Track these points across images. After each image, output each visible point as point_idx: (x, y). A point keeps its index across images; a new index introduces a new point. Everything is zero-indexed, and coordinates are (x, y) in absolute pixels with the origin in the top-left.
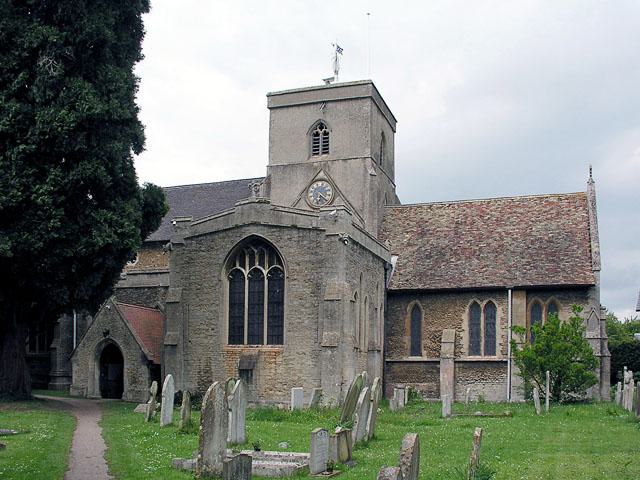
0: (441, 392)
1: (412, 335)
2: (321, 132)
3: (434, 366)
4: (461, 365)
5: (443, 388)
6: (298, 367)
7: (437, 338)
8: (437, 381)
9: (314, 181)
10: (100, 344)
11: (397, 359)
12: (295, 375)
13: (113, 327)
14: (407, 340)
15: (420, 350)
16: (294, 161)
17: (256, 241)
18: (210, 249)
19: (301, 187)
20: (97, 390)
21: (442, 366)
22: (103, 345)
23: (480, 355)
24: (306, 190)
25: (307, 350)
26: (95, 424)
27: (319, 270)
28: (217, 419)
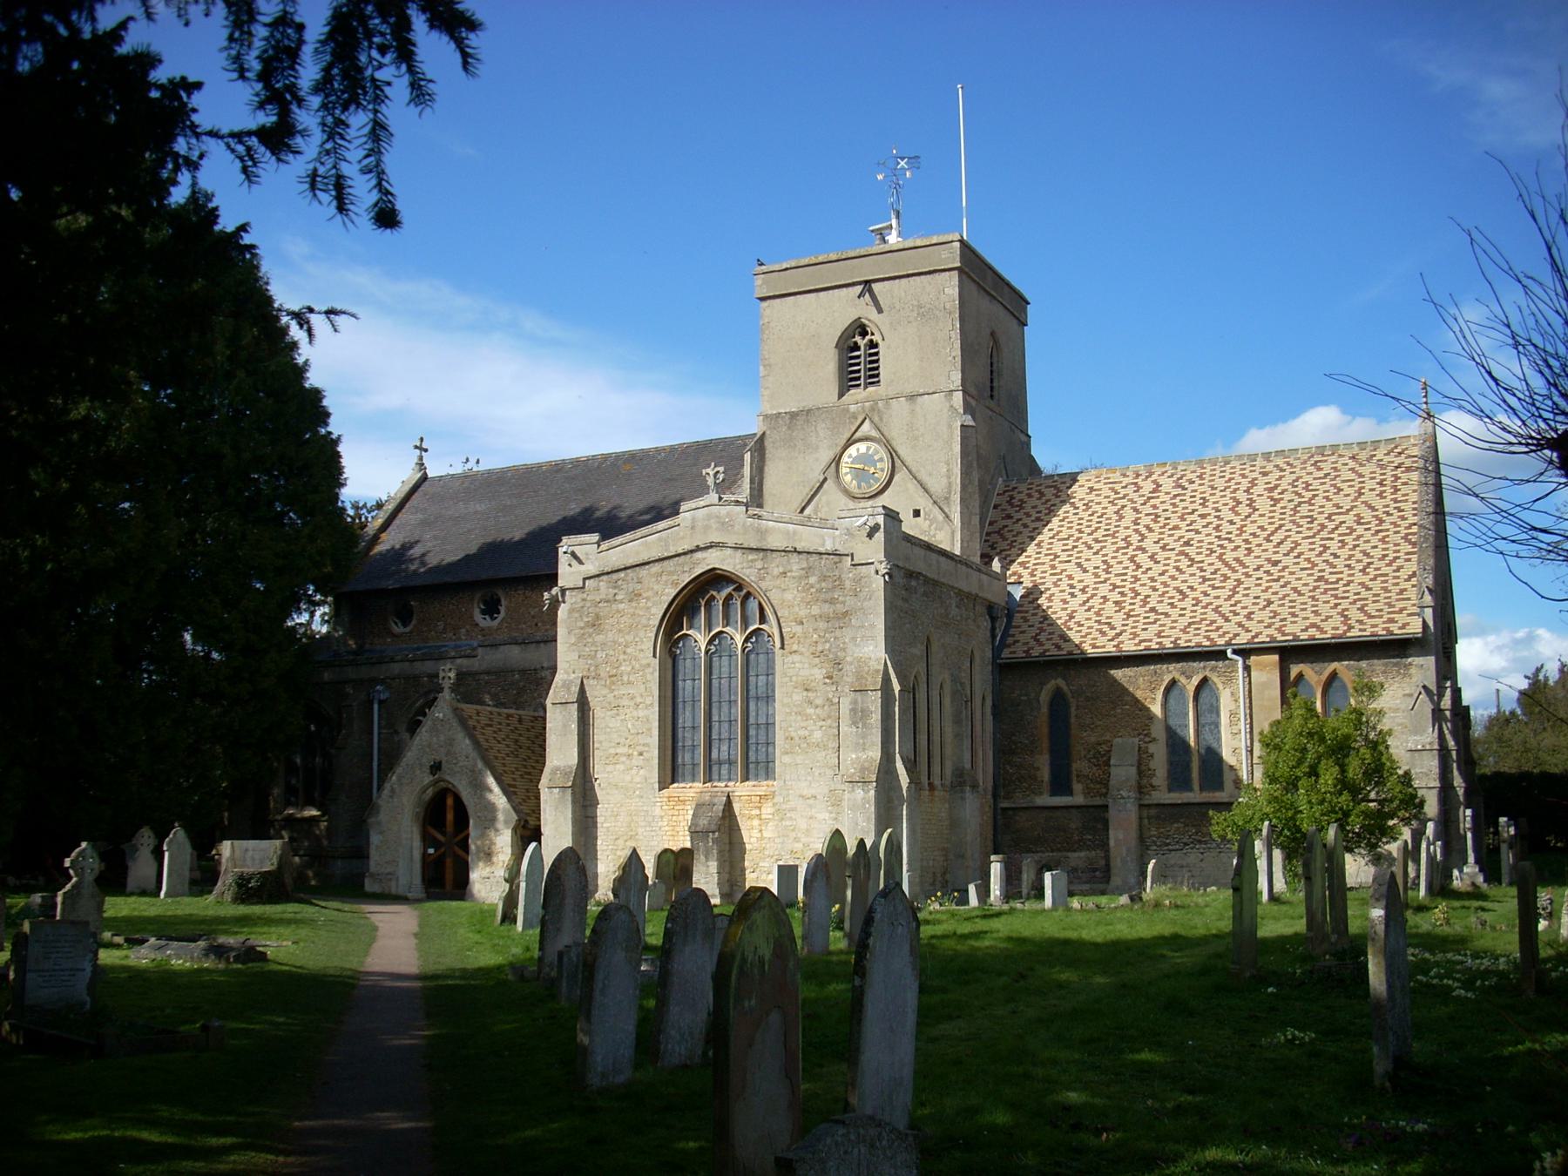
0: (1114, 871)
1: (1052, 752)
2: (862, 342)
3: (1097, 818)
4: (1153, 812)
5: (1116, 863)
6: (802, 824)
7: (1102, 760)
8: (1104, 845)
9: (850, 443)
10: (424, 791)
11: (1022, 803)
12: (797, 840)
13: (448, 753)
14: (1043, 765)
15: (1069, 780)
16: (808, 403)
17: (714, 579)
18: (635, 596)
19: (826, 455)
20: (417, 880)
21: (1112, 813)
22: (430, 792)
23: (1191, 790)
24: (837, 460)
25: (820, 788)
26: (384, 498)
27: (838, 633)
28: (569, 901)
